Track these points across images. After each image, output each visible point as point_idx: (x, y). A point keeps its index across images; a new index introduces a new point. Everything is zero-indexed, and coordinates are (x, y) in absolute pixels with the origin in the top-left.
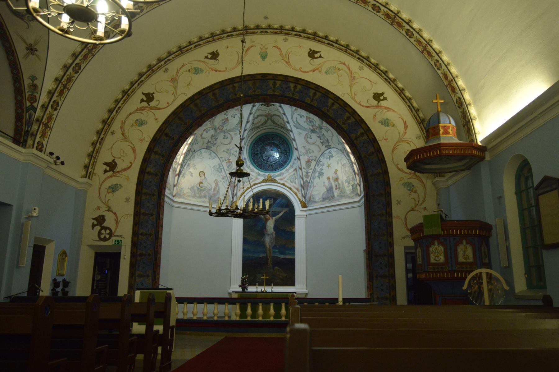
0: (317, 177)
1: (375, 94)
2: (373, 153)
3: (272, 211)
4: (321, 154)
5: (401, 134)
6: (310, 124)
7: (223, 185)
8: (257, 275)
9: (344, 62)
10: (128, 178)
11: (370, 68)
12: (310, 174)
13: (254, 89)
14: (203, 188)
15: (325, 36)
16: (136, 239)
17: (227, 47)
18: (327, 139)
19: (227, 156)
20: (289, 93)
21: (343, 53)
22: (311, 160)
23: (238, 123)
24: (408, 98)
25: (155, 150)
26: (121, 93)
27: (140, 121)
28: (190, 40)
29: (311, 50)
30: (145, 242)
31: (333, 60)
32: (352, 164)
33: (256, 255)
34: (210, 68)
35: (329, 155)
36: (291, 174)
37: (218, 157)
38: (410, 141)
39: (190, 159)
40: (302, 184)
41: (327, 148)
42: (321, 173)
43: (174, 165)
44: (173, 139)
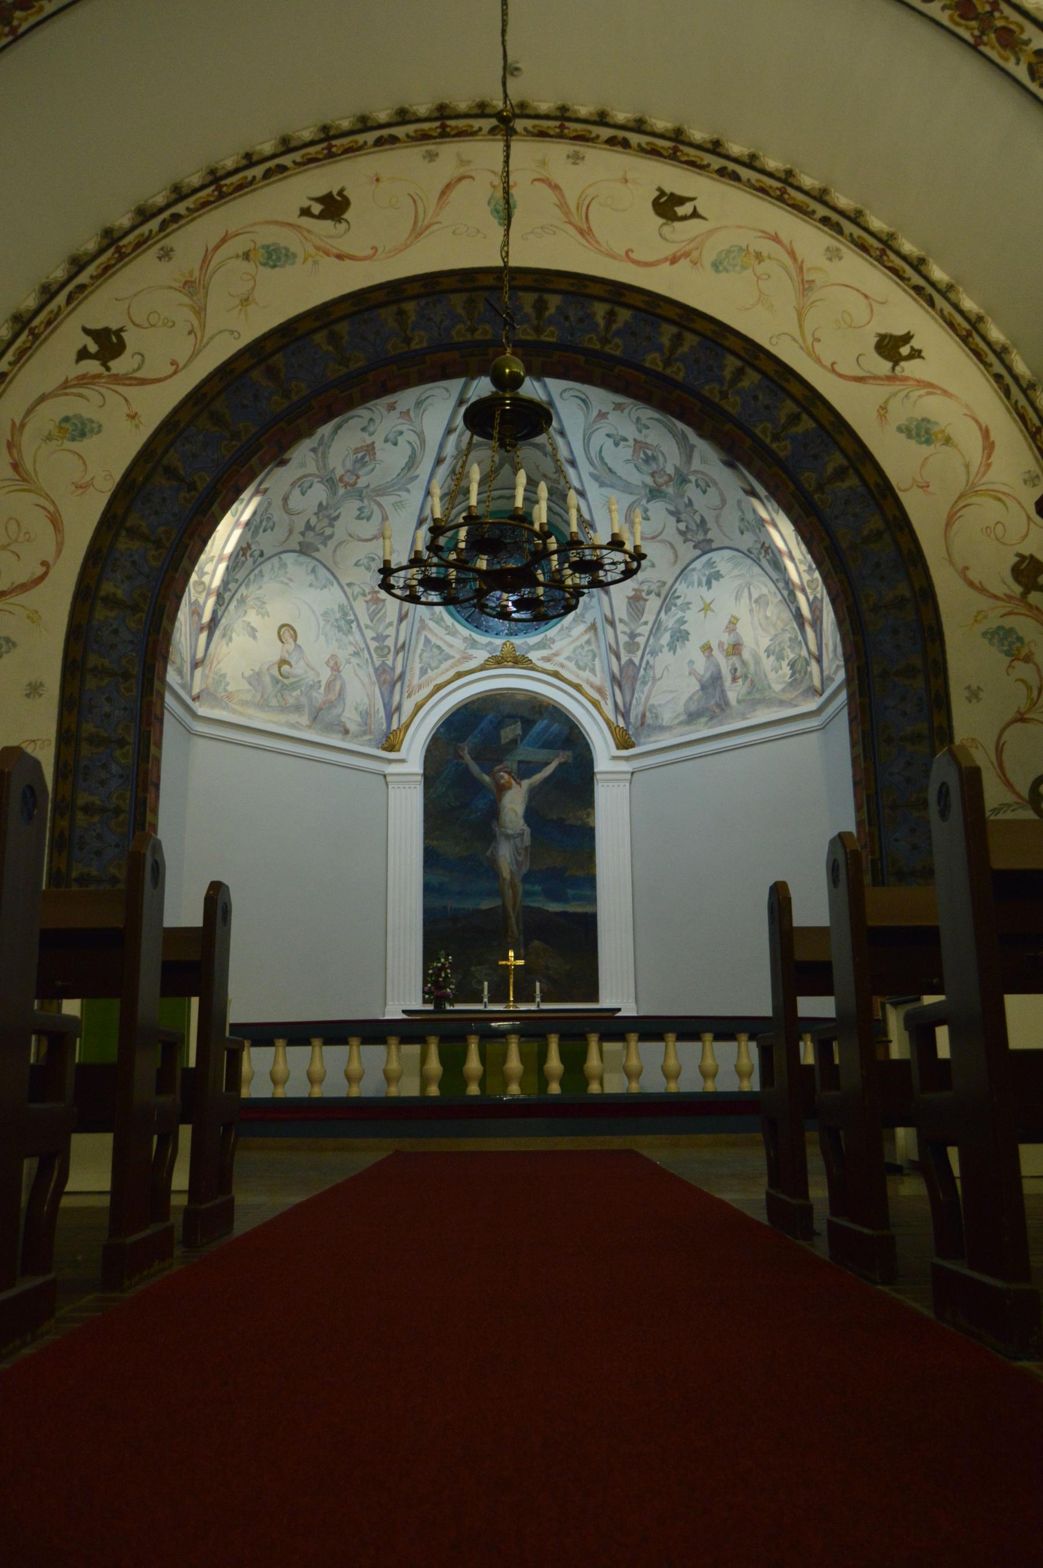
0: (666, 649)
1: (882, 338)
2: (879, 534)
3: (520, 762)
4: (675, 575)
5: (974, 469)
6: (644, 468)
7: (357, 675)
8: (473, 969)
9: (776, 233)
10: (34, 617)
11: (865, 255)
12: (641, 640)
13: (469, 323)
14: (292, 680)
15: (711, 141)
16: (64, 823)
17: (378, 180)
18: (702, 516)
19: (369, 582)
20: (589, 336)
21: (770, 203)
22: (644, 594)
23: (406, 463)
24: (998, 348)
25: (129, 523)
26: (7, 321)
27: (76, 422)
28: (248, 149)
29: (662, 193)
30: (99, 837)
31: (740, 227)
32: (792, 594)
33: (469, 905)
34: (318, 248)
35: (707, 573)
36: (578, 643)
37: (335, 577)
38: (1004, 493)
39: (246, 581)
40: (616, 669)
41: (698, 552)
42: (678, 634)
43: (192, 593)
44: (192, 486)
